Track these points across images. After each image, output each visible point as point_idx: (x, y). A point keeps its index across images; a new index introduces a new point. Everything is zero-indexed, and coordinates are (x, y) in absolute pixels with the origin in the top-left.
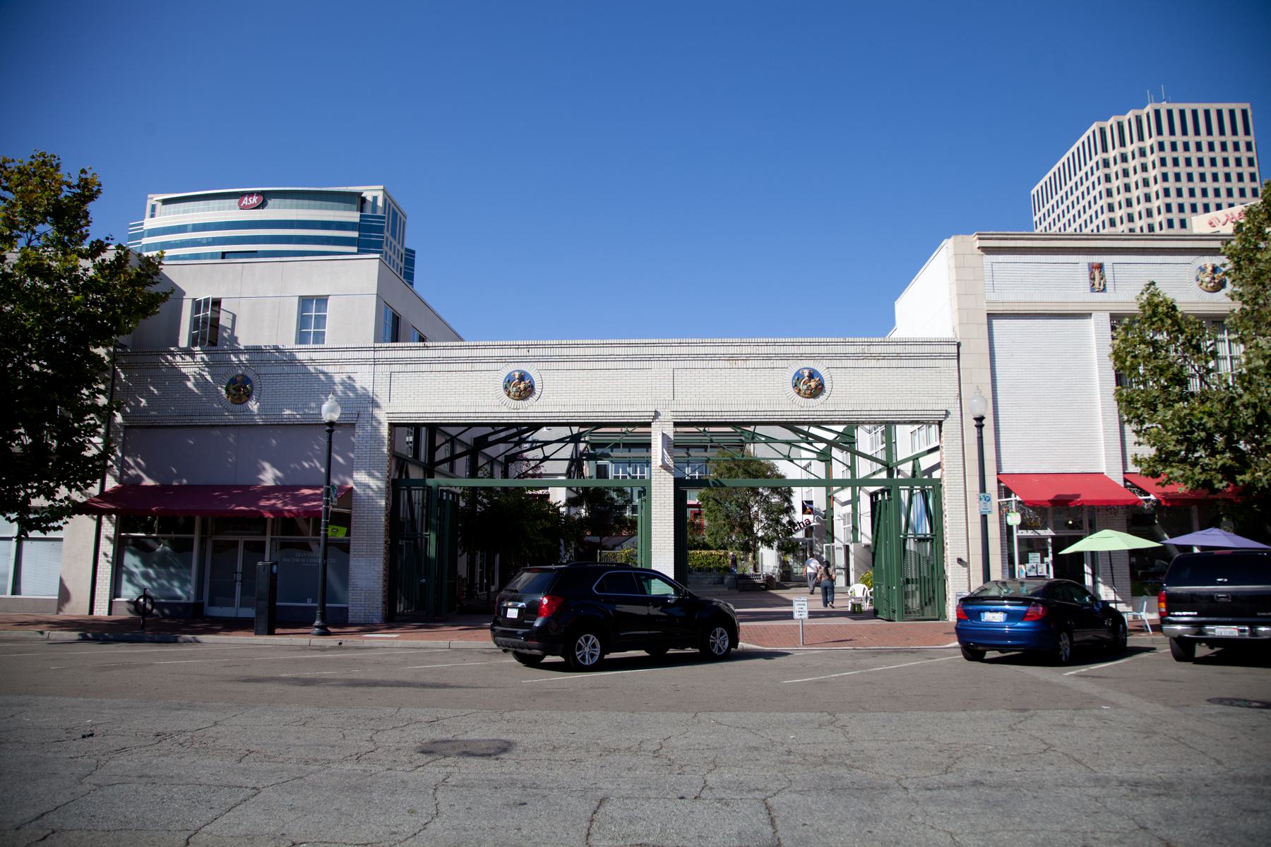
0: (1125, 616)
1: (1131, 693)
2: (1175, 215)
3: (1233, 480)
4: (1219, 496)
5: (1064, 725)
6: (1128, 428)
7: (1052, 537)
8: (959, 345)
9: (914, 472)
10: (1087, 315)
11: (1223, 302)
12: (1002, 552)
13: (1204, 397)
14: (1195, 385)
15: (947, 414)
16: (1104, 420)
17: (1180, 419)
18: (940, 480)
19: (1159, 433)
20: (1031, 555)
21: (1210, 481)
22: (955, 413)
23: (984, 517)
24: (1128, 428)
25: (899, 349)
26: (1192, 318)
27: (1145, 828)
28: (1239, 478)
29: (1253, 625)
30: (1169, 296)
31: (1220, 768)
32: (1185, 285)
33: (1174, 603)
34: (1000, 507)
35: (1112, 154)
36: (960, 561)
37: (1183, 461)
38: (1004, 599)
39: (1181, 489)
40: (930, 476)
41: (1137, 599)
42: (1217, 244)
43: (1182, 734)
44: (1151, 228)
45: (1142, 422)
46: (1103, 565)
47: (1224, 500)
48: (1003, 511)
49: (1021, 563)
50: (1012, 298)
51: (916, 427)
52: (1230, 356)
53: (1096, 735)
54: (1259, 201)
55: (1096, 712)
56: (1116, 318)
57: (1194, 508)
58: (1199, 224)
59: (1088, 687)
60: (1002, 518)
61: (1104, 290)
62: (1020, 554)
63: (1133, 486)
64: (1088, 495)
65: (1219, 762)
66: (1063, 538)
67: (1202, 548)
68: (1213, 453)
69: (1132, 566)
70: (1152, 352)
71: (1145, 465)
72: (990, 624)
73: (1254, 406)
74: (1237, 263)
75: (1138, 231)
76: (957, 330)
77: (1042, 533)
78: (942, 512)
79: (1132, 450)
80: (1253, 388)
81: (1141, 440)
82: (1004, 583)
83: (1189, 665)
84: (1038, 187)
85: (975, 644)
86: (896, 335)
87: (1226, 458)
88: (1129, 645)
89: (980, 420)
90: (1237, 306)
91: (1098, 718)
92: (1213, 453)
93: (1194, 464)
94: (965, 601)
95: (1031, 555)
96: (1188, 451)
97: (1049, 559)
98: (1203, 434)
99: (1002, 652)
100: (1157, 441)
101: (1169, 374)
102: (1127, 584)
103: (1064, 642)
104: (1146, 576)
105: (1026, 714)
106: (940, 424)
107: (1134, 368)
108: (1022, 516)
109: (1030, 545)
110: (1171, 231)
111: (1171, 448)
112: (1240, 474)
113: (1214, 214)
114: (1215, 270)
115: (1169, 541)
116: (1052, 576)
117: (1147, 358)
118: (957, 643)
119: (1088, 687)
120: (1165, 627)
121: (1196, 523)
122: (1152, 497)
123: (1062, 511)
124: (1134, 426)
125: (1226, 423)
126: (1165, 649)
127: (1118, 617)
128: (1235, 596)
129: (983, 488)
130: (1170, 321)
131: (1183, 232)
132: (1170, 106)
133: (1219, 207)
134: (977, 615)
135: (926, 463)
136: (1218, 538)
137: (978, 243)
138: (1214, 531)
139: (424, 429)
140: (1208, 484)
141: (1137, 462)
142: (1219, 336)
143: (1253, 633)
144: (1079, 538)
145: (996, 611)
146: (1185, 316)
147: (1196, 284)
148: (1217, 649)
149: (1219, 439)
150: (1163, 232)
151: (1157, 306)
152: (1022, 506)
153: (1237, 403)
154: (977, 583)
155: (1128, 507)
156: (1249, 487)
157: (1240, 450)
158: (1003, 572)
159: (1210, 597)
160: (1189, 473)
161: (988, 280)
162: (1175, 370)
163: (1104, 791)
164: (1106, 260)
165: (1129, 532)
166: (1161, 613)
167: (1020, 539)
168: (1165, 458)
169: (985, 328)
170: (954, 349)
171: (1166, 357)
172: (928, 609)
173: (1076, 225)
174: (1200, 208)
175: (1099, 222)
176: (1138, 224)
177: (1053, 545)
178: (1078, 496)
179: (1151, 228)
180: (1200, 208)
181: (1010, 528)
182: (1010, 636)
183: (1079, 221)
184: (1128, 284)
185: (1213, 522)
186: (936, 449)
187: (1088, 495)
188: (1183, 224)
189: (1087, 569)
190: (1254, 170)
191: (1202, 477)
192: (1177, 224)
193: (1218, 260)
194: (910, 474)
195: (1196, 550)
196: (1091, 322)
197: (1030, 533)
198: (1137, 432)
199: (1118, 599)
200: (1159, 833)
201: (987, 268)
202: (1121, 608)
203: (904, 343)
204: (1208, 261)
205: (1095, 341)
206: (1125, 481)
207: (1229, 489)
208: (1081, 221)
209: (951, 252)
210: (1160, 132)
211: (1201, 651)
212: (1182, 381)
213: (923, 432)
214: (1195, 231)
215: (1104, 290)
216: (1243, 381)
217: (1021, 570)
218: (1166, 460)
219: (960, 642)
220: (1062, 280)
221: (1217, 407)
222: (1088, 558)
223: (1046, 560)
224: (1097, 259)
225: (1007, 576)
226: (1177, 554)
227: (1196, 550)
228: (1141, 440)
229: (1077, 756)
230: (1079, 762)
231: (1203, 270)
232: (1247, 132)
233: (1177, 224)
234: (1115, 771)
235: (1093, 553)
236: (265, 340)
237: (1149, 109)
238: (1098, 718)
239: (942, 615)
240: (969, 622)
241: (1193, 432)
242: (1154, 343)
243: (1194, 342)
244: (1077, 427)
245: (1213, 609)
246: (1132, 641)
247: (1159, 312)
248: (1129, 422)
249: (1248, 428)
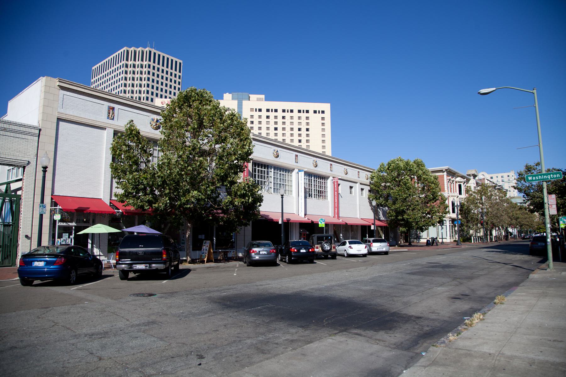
0: (103, 262)
1: (99, 295)
2: (150, 96)
3: (151, 206)
4: (146, 212)
5: (65, 313)
6: (114, 181)
7: (75, 226)
8: (40, 130)
9: (6, 190)
10: (103, 128)
11: (158, 135)
12: (50, 232)
13: (145, 172)
14: (143, 166)
15: (29, 163)
16: (105, 175)
17: (134, 179)
18: (20, 195)
19: (126, 184)
20: (64, 234)
21: (143, 206)
22: (33, 163)
23: (41, 216)
24: (115, 181)
25: (6, 126)
26: (145, 139)
27: (92, 354)
28: (154, 205)
29: (150, 264)
30: (138, 128)
31: (128, 323)
32: (146, 125)
33: (122, 256)
34: (51, 211)
35: (130, 63)
36: (27, 236)
37: (134, 197)
38: (46, 255)
39: (132, 209)
40: (16, 193)
41: (110, 254)
42: (159, 111)
43: (116, 310)
44: (140, 99)
45: (120, 179)
46: (96, 240)
47: (148, 214)
48: (52, 213)
49: (58, 238)
50: (71, 114)
51: (11, 167)
52: (157, 157)
53: (79, 315)
54: (176, 98)
55: (82, 305)
56: (115, 133)
57: (137, 216)
58: (158, 102)
59: (81, 294)
60: (51, 216)
61: (113, 119)
62: (58, 233)
63: (114, 205)
64: (93, 208)
65: (128, 320)
66: (81, 227)
67: (138, 233)
68: (145, 194)
69: (109, 240)
70: (128, 149)
71: (119, 197)
72: (37, 267)
73: (162, 177)
74: (165, 120)
75: (134, 98)
76: (40, 122)
77: (70, 224)
78: (19, 211)
79: (115, 190)
80: (162, 170)
81: (119, 186)
82: (48, 247)
83: (126, 281)
84: (96, 67)
85: (28, 277)
86: (6, 118)
87: (149, 197)
88: (103, 274)
89: (45, 169)
90: (163, 137)
91: (82, 308)
92: (145, 194)
93: (138, 199)
94: (24, 256)
95: (64, 234)
96: (136, 193)
97: (72, 236)
98: (143, 186)
99: (42, 280)
100: (125, 188)
101: (133, 160)
102: (106, 248)
103: (73, 274)
104: (115, 244)
105: (48, 309)
106: (24, 167)
107: (120, 155)
108: (62, 216)
109: (67, 230)
110: (147, 102)
111: (130, 191)
112: (155, 203)
113: (163, 99)
114: (157, 121)
115: (125, 230)
116: (73, 245)
117: (126, 152)
118: (18, 278)
119: (81, 294)
120: (117, 266)
121: (136, 223)
122: (120, 211)
123: (80, 214)
124: (116, 180)
125: (151, 183)
126: (117, 275)
127: (100, 262)
128: (145, 253)
129: (42, 201)
130: (136, 138)
131: (152, 103)
132: (156, 51)
133: (166, 97)
134: (31, 263)
135: (14, 186)
136: (143, 229)
137: (58, 83)
138: (143, 226)
139: (543, 244)
140: (142, 207)
141: (116, 195)
142: (155, 148)
143: (150, 267)
144: (88, 227)
145: (41, 261)
146: (143, 137)
147: (149, 125)
148: (137, 274)
149: (149, 189)
150: (144, 101)
151: (132, 130)
152: (62, 211)
153: (156, 176)
154: (35, 246)
155: (110, 214)
156: (157, 209)
157: (155, 194)
158: (49, 242)
159: (136, 253)
160: (136, 202)
161: (60, 102)
162: (136, 159)
163: (77, 341)
164: (116, 106)
165: (109, 226)
166: (116, 260)
167: (59, 227)
168: (127, 195)
169: (56, 124)
170: (37, 132)
171: (133, 152)
172: (7, 261)
173: (109, 89)
174: (159, 96)
175: (119, 90)
176: (135, 95)
177: (75, 230)
178: (89, 208)
179: (140, 99)
180: (159, 96)
181: (55, 221)
182: (47, 273)
183: (111, 87)
184: (123, 118)
185: (144, 223)
186: (21, 180)
187: (93, 208)
188: (152, 100)
189: (90, 241)
190: (180, 87)
191: (140, 204)
192: (150, 99)
193: (159, 117)
194: (4, 191)
195: (135, 234)
196: (105, 132)
197: (64, 224)
198: (117, 183)
199: (101, 254)
200: (98, 355)
201: (61, 96)
202: (102, 258)
203: (10, 123)
204: (156, 117)
205: (106, 140)
206: (110, 203)
207: (150, 210)
208: (112, 87)
209: (44, 83)
210: (150, 61)
211: (131, 275)
212: (136, 163)
213: (15, 171)
214: (156, 105)
215: (113, 119)
216: (159, 167)
217: (58, 241)
218: (128, 196)
219: (19, 277)
220: (96, 111)
221: (149, 176)
222: (90, 236)
223: (71, 237)
224: (112, 105)
225: (51, 243)
226: (127, 234)
227: (135, 234)
228: (119, 186)
229: (68, 326)
230: (69, 329)
231: (153, 120)
232: (180, 72)
233: (150, 99)
234: (84, 331)
235: (93, 234)
236: (553, 214)
237: (148, 49)
238: (82, 308)
239: (14, 264)
240: (26, 267)
241: (139, 185)
242: (129, 146)
243: (145, 148)
244: (91, 177)
245: (137, 258)
246: (104, 273)
247: (133, 133)
248: (115, 178)
249: (159, 186)
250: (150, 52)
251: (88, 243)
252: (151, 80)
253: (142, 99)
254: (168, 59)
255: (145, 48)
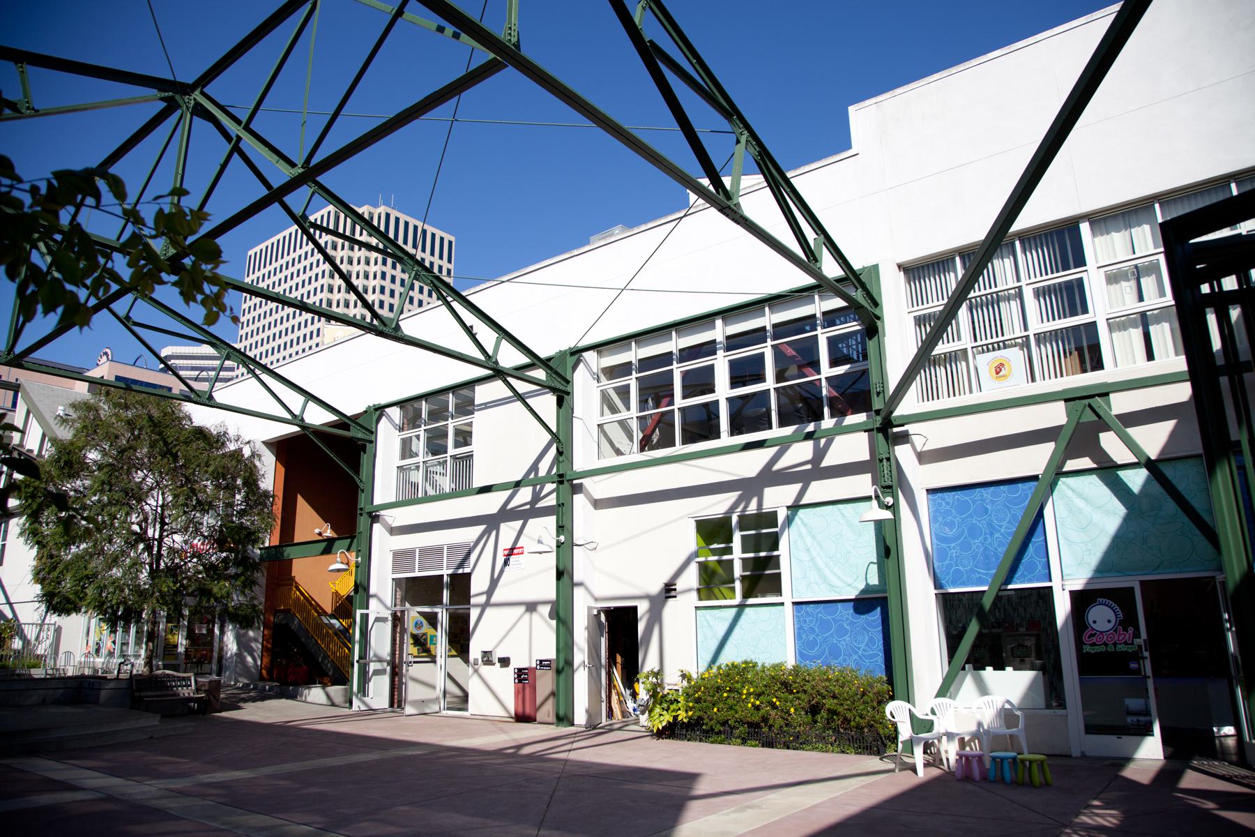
232: (450, 261)
250: (388, 216)
251: (1220, 621)
252: (388, 278)
253: (334, 304)
254: (397, 220)
255: (376, 206)
